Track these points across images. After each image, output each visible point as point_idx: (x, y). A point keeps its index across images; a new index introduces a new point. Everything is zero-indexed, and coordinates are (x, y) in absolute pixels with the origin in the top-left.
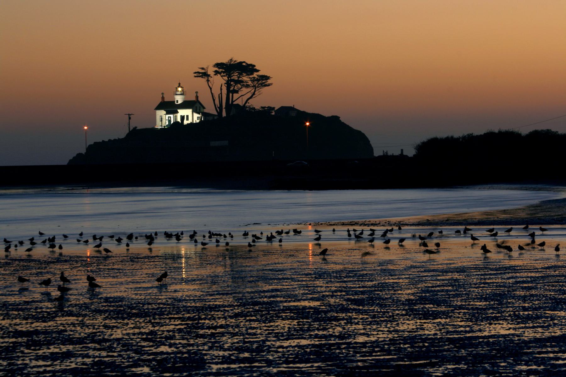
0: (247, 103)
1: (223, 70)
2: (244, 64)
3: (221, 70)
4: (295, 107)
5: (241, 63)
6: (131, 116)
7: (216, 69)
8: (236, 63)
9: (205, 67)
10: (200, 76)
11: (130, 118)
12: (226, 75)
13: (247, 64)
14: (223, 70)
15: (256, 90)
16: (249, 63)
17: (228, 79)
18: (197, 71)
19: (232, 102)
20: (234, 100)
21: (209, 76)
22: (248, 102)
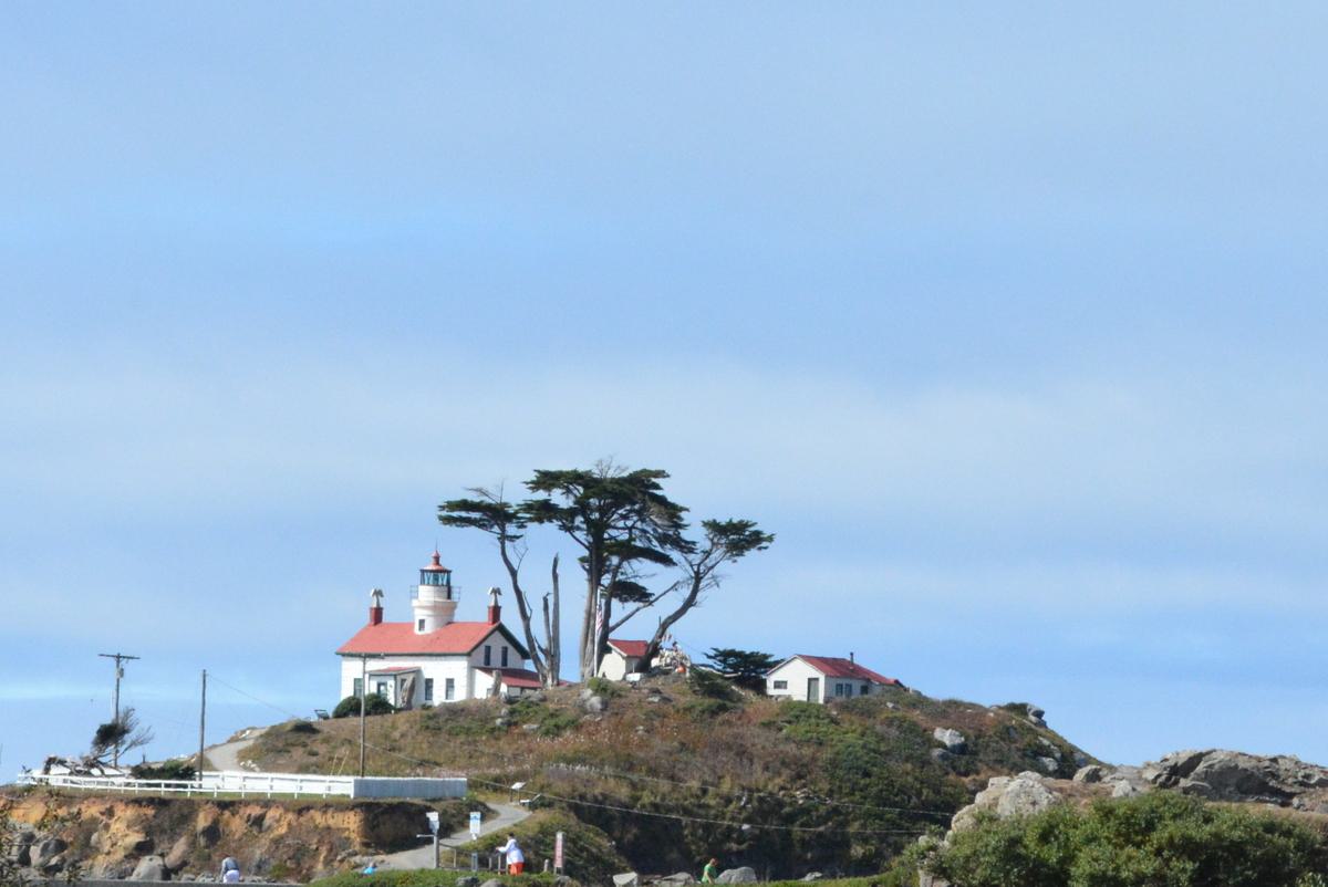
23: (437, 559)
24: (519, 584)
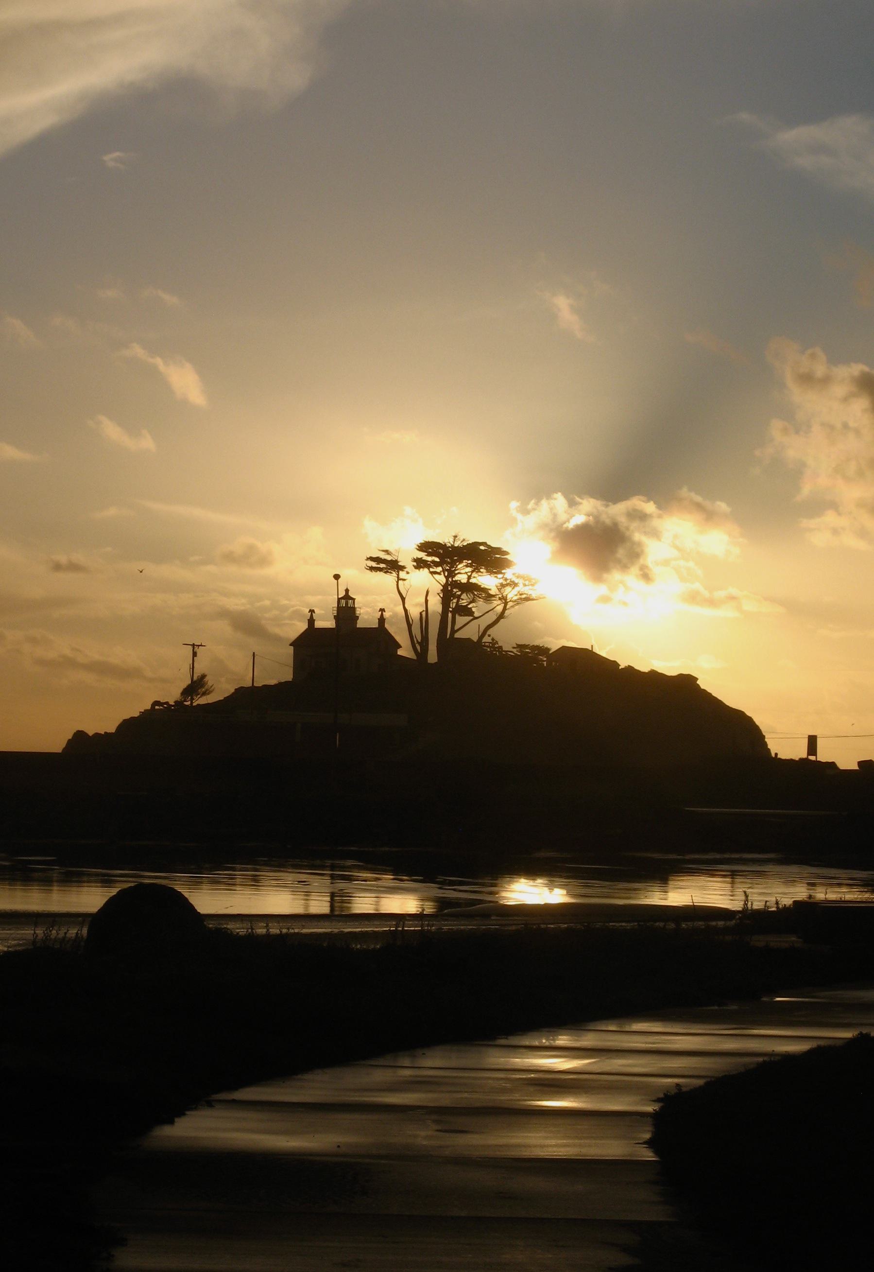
0: (487, 636)
1: (437, 559)
2: (482, 548)
3: (429, 559)
4: (594, 651)
5: (476, 545)
6: (199, 651)
7: (422, 555)
8: (465, 544)
9: (391, 549)
10: (380, 569)
11: (195, 654)
12: (444, 571)
13: (489, 546)
14: (437, 559)
15: (508, 607)
16: (494, 545)
17: (447, 580)
18: (374, 556)
19: (453, 632)
20: (456, 628)
21: (402, 568)
22: (488, 633)
23: (812, 741)
24: (406, 606)
